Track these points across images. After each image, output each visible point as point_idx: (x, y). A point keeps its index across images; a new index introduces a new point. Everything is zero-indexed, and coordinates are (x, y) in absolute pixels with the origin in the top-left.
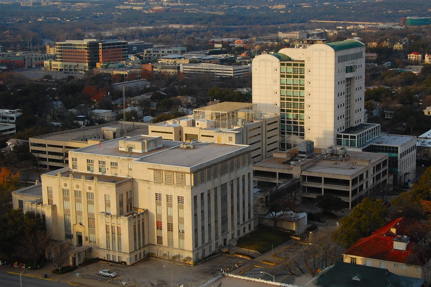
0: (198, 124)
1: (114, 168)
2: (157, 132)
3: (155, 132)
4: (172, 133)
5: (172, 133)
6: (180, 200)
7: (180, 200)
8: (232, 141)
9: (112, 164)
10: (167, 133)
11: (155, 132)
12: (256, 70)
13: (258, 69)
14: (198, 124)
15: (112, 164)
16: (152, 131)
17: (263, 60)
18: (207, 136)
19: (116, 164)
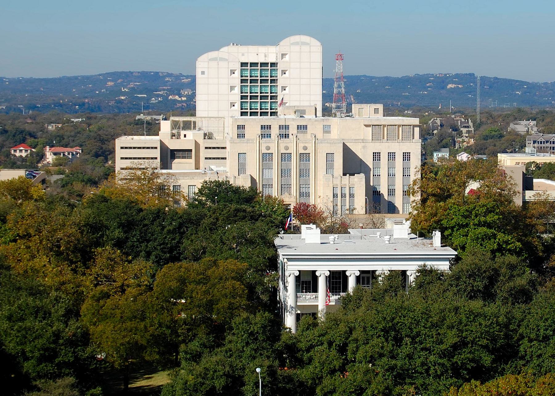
0: (185, 136)
1: (302, 132)
2: (130, 148)
3: (126, 148)
4: (156, 148)
5: (156, 148)
6: (406, 156)
7: (406, 156)
8: (378, 113)
9: (299, 127)
10: (148, 148)
11: (126, 148)
12: (203, 73)
13: (206, 73)
14: (185, 136)
15: (299, 127)
16: (122, 148)
17: (297, 43)
18: (214, 148)
19: (305, 127)
